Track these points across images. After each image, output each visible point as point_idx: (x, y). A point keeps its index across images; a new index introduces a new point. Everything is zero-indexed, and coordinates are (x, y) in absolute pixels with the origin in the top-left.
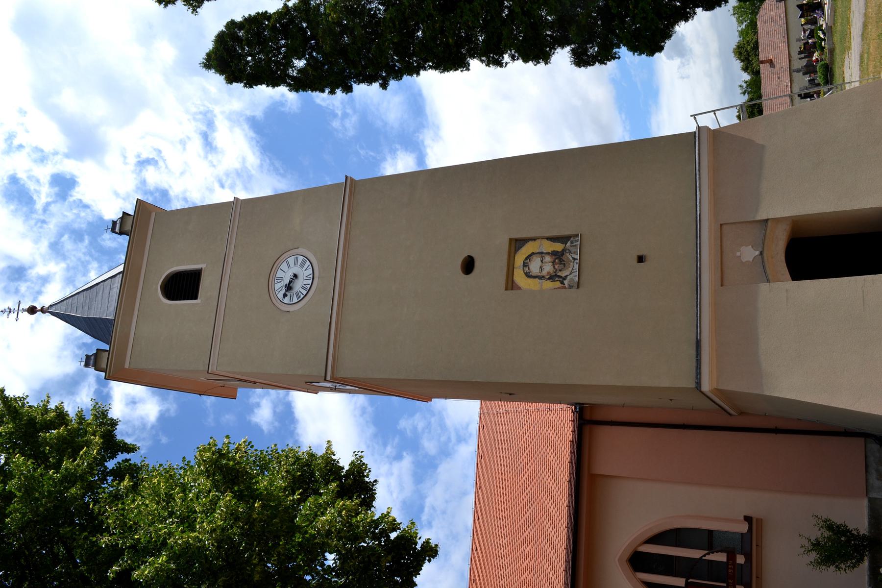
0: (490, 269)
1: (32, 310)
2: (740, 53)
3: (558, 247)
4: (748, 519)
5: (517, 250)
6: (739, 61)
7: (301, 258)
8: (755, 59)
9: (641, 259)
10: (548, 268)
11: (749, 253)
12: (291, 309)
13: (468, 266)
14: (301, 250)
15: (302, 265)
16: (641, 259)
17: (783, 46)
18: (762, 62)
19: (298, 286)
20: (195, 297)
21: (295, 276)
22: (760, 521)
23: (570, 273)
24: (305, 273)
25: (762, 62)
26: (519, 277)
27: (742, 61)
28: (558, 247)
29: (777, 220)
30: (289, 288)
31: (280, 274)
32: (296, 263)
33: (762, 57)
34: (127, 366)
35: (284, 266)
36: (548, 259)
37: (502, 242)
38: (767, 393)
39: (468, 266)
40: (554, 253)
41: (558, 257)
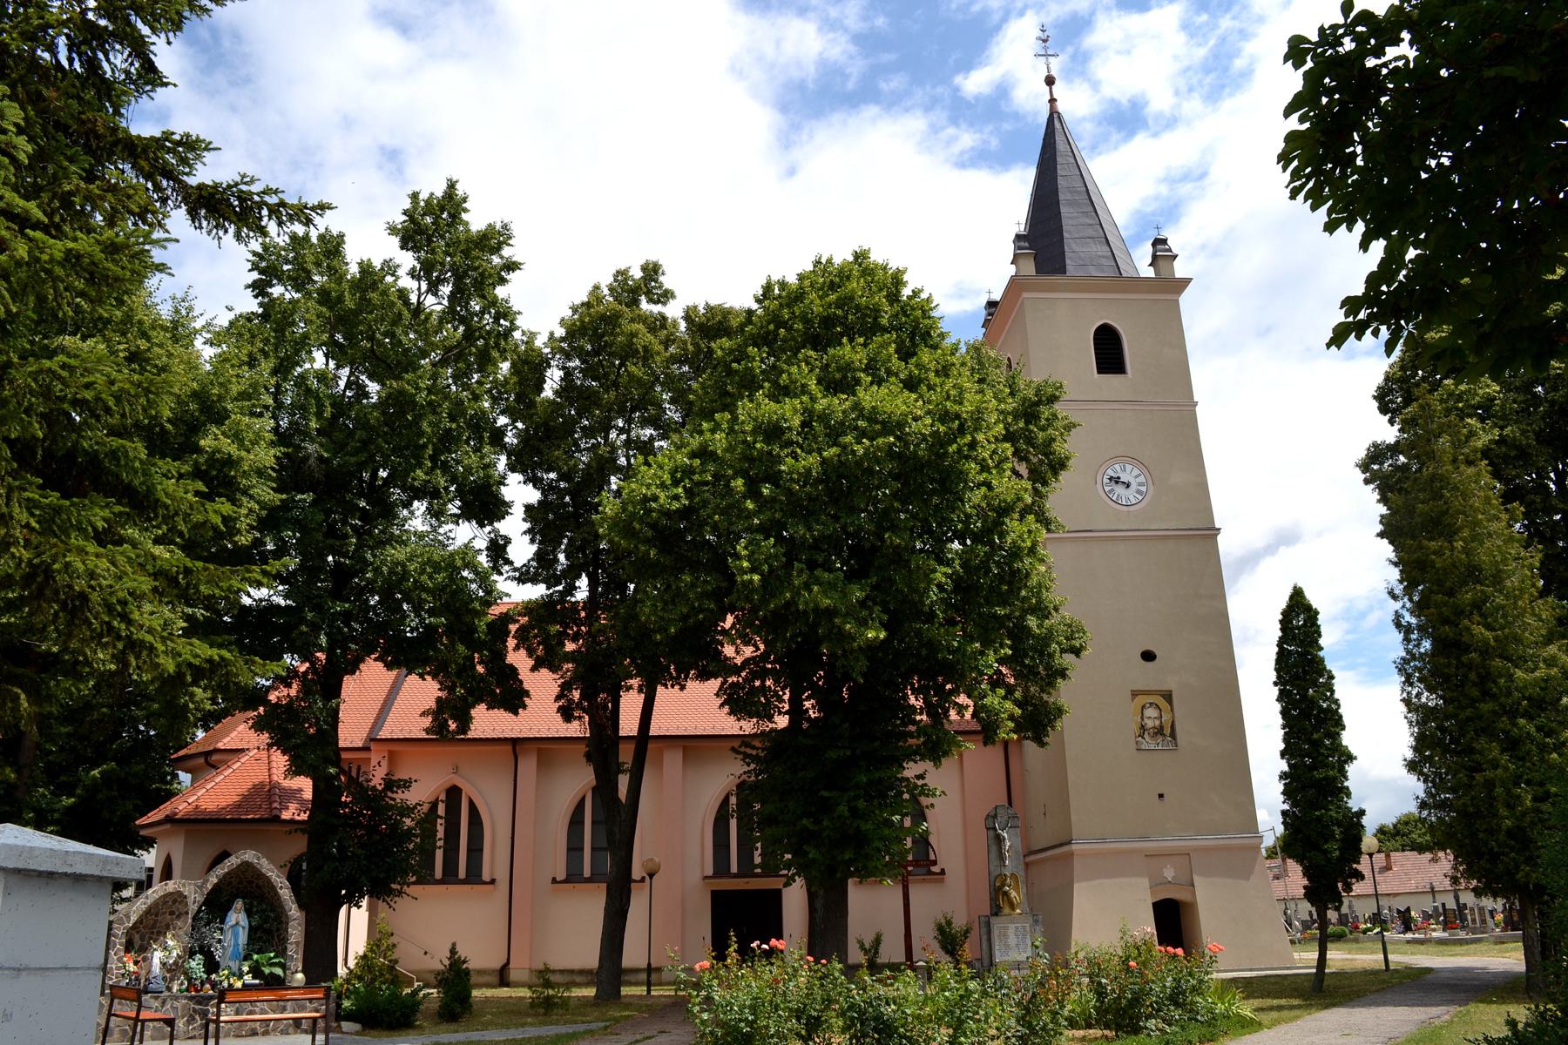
0: (1147, 676)
1: (1050, 81)
2: (1406, 823)
3: (1167, 731)
4: (943, 872)
5: (1163, 696)
6: (1394, 821)
7: (1144, 489)
8: (1397, 845)
9: (1161, 796)
10: (1150, 724)
11: (1169, 874)
12: (1099, 486)
13: (1148, 656)
14: (1151, 488)
15: (1139, 492)
16: (1161, 796)
17: (1411, 886)
18: (1388, 856)
19: (1120, 489)
20: (1100, 371)
21: (1128, 486)
22: (942, 881)
23: (1148, 742)
24: (1130, 495)
25: (1388, 856)
26: (1141, 700)
27: (1395, 826)
28: (1167, 731)
29: (1194, 893)
30: (1117, 481)
31: (1129, 467)
32: (1140, 484)
33: (1395, 856)
34: (1025, 295)
35: (1136, 472)
36: (1157, 723)
37: (1170, 684)
38: (1076, 886)
39: (1148, 656)
40: (1162, 727)
41: (1159, 731)
